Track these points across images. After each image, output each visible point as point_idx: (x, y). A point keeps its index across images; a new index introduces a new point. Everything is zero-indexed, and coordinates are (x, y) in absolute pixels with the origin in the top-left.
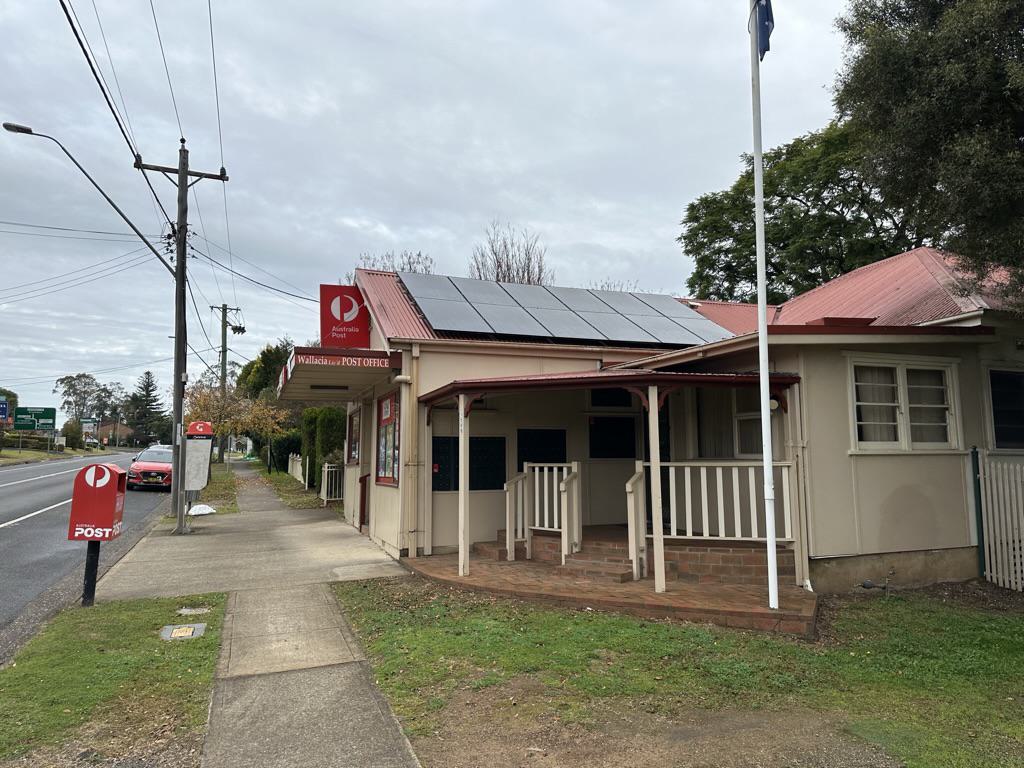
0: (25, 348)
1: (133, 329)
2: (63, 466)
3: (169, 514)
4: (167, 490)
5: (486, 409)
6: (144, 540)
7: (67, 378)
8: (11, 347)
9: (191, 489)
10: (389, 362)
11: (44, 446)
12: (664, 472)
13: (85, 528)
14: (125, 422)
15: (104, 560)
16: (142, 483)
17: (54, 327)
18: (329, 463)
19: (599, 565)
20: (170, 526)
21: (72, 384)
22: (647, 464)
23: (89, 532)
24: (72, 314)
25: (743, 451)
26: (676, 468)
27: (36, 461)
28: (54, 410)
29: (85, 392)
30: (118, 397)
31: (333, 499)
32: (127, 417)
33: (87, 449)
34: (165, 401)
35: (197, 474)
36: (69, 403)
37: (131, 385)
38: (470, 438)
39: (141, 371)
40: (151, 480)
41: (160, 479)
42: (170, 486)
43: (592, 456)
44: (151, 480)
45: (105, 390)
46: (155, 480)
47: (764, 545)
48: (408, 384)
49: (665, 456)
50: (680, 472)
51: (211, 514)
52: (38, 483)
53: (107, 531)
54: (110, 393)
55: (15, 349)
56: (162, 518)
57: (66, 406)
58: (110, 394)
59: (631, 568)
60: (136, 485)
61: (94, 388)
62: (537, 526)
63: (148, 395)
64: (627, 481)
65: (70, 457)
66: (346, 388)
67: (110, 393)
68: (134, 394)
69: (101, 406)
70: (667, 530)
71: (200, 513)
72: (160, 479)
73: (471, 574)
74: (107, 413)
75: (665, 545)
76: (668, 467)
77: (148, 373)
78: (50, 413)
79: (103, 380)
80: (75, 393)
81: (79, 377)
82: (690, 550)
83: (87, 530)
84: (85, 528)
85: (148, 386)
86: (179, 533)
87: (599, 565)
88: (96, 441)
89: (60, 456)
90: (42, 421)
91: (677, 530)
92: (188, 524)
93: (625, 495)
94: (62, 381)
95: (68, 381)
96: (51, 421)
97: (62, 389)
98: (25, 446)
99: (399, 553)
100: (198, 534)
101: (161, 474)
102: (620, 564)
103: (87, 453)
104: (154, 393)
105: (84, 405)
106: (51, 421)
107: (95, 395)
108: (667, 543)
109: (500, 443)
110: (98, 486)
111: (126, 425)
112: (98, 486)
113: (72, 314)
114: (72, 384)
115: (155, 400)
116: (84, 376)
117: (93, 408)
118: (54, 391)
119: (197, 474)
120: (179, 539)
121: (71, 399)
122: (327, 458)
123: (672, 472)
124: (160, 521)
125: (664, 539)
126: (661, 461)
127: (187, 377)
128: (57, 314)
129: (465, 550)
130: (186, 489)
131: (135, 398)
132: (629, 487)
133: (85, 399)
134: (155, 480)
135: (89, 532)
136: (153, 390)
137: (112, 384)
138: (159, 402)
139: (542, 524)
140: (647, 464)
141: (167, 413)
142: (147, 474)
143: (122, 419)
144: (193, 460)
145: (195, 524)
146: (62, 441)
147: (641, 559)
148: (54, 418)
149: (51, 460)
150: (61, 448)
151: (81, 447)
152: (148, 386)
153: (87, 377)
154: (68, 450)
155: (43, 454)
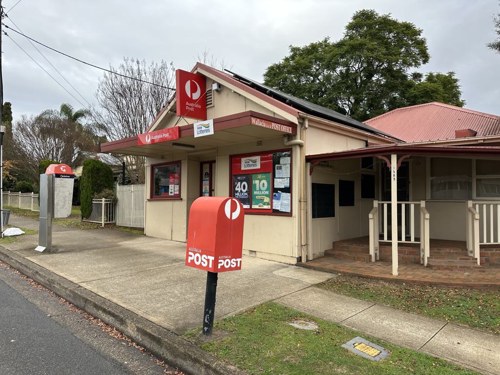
5: (328, 166)
10: (292, 129)
12: (399, 207)
15: (199, 295)
18: (106, 198)
19: (453, 262)
22: (389, 202)
23: (227, 263)
25: (478, 195)
26: (406, 204)
31: (111, 222)
38: (314, 186)
43: (362, 197)
47: (390, 244)
48: (301, 146)
49: (402, 196)
50: (408, 208)
51: (23, 234)
59: (477, 262)
62: (485, 242)
64: (369, 213)
66: (193, 146)
70: (400, 238)
73: (399, 275)
75: (398, 246)
76: (401, 204)
82: (496, 250)
87: (453, 262)
91: (415, 238)
93: (368, 219)
102: (469, 261)
108: (399, 245)
109: (330, 188)
119: (64, 205)
122: (103, 194)
123: (403, 206)
125: (398, 243)
126: (398, 201)
132: (370, 216)
135: (227, 263)
139: (489, 240)
140: (389, 202)
144: (60, 194)
147: (376, 254)
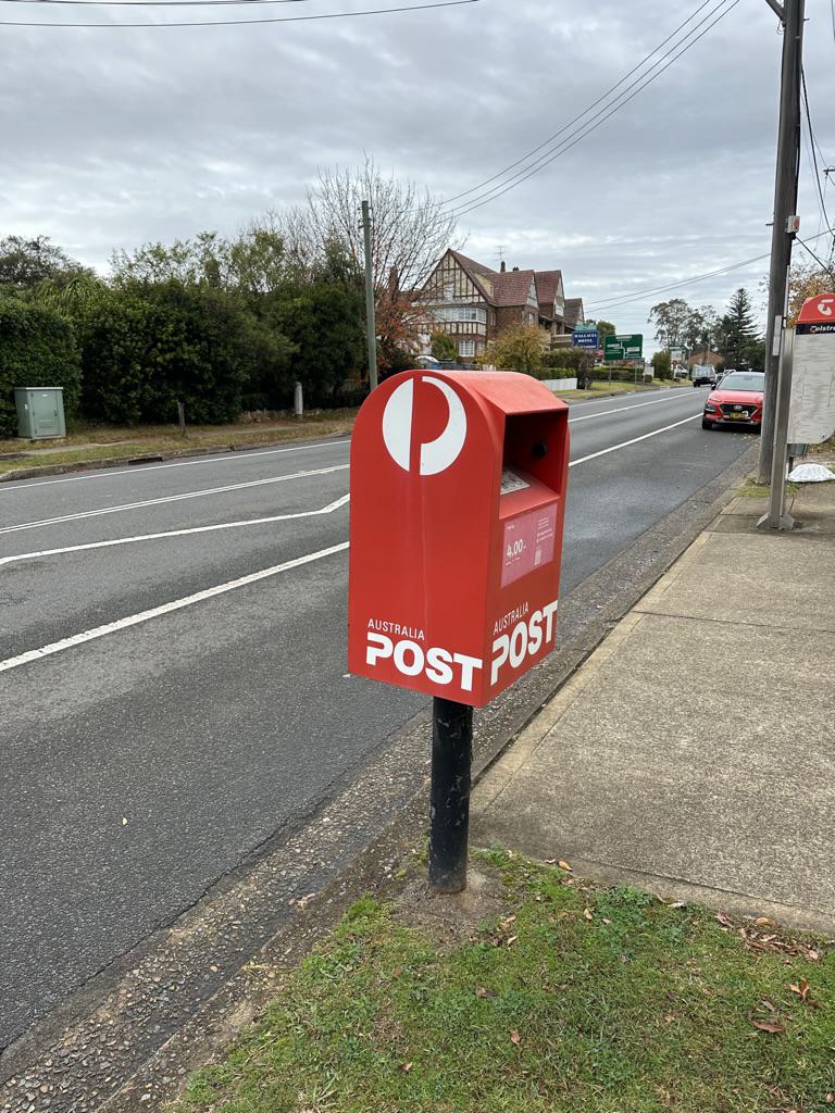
0: (629, 281)
1: (731, 245)
2: (627, 401)
3: (755, 474)
4: (755, 430)
6: (704, 538)
7: (661, 305)
8: (616, 281)
9: (798, 441)
11: (633, 376)
13: (395, 639)
14: (716, 349)
16: (722, 421)
17: (652, 254)
20: (752, 506)
21: (666, 312)
24: (670, 237)
27: (623, 393)
28: (640, 337)
29: (677, 320)
30: (709, 323)
32: (718, 344)
33: (675, 380)
34: (759, 320)
35: (815, 410)
36: (661, 332)
37: (723, 307)
39: (734, 291)
40: (734, 415)
41: (746, 415)
42: (760, 424)
44: (734, 415)
45: (696, 316)
46: (740, 416)
51: (829, 481)
52: (608, 418)
53: (470, 664)
54: (702, 318)
55: (620, 282)
56: (742, 484)
57: (660, 336)
58: (701, 319)
60: (714, 422)
61: (687, 314)
63: (741, 317)
65: (657, 388)
67: (702, 318)
68: (726, 317)
69: (693, 333)
71: (809, 479)
72: (746, 415)
74: (698, 340)
77: (741, 291)
78: (637, 340)
79: (694, 304)
80: (667, 321)
81: (672, 303)
83: (404, 645)
84: (395, 639)
85: (741, 306)
86: (772, 528)
88: (685, 371)
89: (646, 388)
90: (629, 350)
92: (789, 503)
94: (656, 309)
95: (661, 309)
96: (638, 349)
97: (656, 317)
98: (615, 377)
99: (652, 357)
100: (812, 535)
101: (748, 407)
103: (675, 384)
104: (746, 314)
105: (676, 333)
106: (638, 349)
107: (686, 321)
110: (425, 471)
111: (717, 352)
112: (425, 471)
113: (670, 237)
114: (666, 312)
115: (748, 323)
116: (676, 301)
117: (685, 336)
118: (649, 321)
120: (773, 544)
121: (664, 328)
124: (741, 494)
127: (797, 223)
128: (654, 239)
129: (748, 398)
130: (790, 440)
131: (726, 321)
133: (677, 326)
134: (740, 416)
135: (409, 658)
136: (746, 311)
137: (703, 308)
138: (752, 324)
141: (761, 337)
142: (728, 407)
143: (713, 346)
145: (804, 505)
146: (650, 371)
148: (640, 346)
149: (637, 391)
150: (649, 378)
151: (669, 378)
152: (741, 306)
153: (680, 303)
154: (656, 381)
155: (630, 385)
